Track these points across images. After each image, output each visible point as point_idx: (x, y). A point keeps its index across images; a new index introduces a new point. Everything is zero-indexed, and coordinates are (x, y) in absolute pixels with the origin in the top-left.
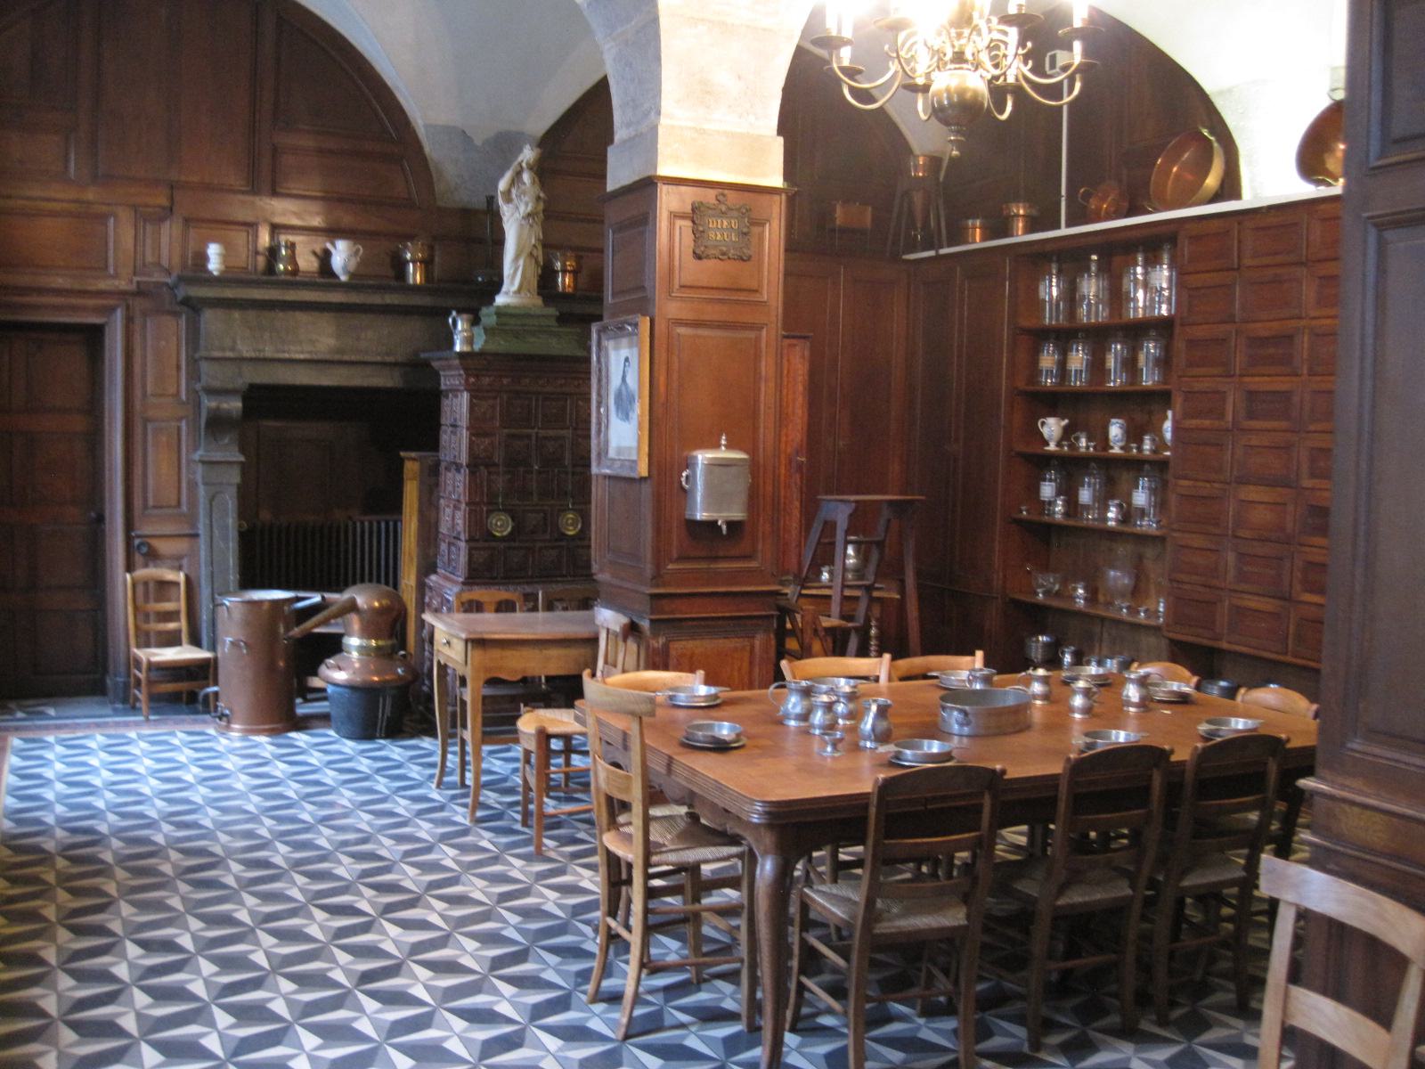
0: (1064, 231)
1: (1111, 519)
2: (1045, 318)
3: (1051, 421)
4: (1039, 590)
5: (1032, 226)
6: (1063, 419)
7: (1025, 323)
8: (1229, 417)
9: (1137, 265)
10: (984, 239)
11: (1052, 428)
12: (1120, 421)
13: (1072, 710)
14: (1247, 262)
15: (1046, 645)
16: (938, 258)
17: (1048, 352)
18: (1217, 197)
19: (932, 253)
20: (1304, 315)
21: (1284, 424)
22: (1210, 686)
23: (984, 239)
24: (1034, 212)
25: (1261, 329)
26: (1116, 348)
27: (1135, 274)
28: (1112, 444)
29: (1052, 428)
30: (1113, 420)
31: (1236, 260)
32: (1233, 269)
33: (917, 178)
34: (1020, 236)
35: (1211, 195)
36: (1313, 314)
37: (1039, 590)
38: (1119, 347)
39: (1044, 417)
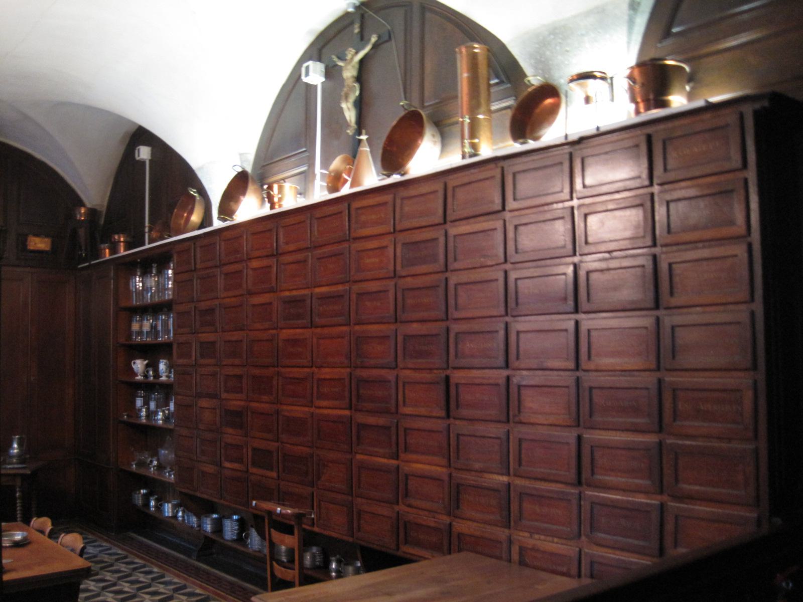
0: (147, 246)
1: (160, 420)
2: (133, 301)
3: (138, 362)
4: (133, 463)
5: (129, 246)
6: (145, 360)
7: (123, 304)
8: (194, 358)
9: (169, 268)
10: (125, 250)
11: (139, 365)
12: (165, 361)
13: (20, 491)
14: (198, 266)
15: (144, 495)
16: (90, 266)
17: (136, 321)
18: (201, 226)
19: (87, 264)
20: (219, 297)
21: (212, 361)
22: (205, 519)
23: (125, 250)
24: (128, 239)
25: (203, 305)
26: (162, 318)
27: (168, 274)
28: (161, 375)
29: (139, 365)
30: (161, 360)
31: (193, 266)
32: (191, 271)
33: (80, 220)
34: (122, 252)
35: (198, 225)
36: (222, 296)
37: (133, 463)
38: (164, 317)
39: (135, 359)
